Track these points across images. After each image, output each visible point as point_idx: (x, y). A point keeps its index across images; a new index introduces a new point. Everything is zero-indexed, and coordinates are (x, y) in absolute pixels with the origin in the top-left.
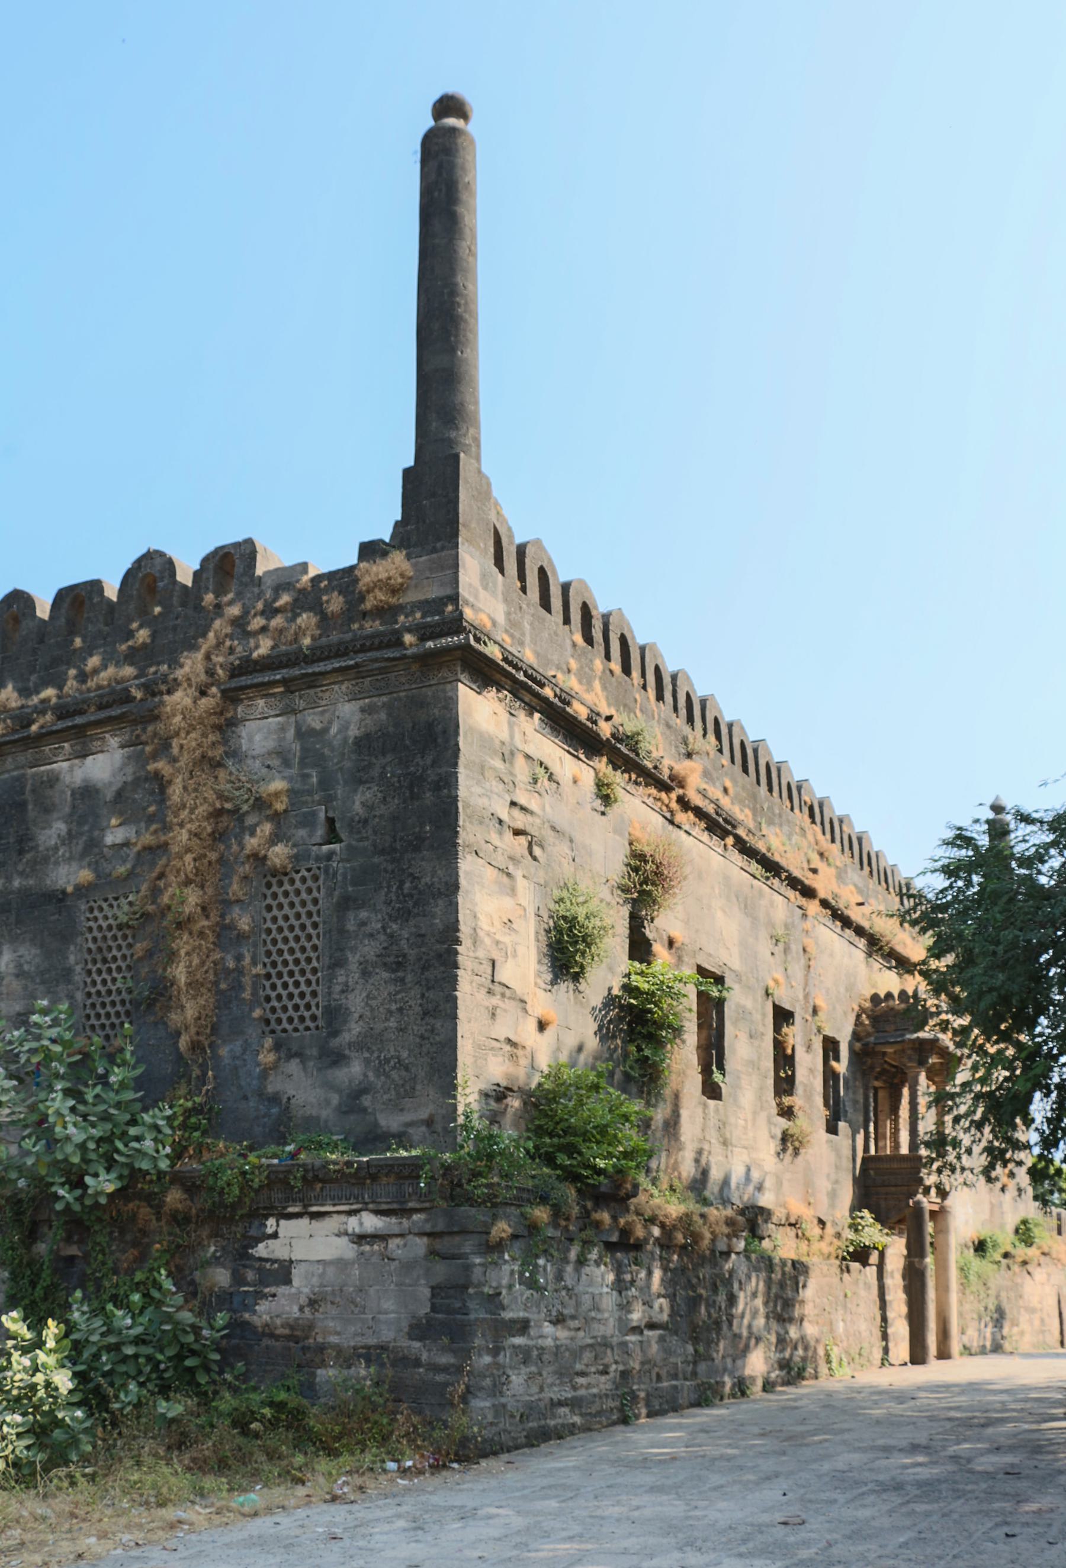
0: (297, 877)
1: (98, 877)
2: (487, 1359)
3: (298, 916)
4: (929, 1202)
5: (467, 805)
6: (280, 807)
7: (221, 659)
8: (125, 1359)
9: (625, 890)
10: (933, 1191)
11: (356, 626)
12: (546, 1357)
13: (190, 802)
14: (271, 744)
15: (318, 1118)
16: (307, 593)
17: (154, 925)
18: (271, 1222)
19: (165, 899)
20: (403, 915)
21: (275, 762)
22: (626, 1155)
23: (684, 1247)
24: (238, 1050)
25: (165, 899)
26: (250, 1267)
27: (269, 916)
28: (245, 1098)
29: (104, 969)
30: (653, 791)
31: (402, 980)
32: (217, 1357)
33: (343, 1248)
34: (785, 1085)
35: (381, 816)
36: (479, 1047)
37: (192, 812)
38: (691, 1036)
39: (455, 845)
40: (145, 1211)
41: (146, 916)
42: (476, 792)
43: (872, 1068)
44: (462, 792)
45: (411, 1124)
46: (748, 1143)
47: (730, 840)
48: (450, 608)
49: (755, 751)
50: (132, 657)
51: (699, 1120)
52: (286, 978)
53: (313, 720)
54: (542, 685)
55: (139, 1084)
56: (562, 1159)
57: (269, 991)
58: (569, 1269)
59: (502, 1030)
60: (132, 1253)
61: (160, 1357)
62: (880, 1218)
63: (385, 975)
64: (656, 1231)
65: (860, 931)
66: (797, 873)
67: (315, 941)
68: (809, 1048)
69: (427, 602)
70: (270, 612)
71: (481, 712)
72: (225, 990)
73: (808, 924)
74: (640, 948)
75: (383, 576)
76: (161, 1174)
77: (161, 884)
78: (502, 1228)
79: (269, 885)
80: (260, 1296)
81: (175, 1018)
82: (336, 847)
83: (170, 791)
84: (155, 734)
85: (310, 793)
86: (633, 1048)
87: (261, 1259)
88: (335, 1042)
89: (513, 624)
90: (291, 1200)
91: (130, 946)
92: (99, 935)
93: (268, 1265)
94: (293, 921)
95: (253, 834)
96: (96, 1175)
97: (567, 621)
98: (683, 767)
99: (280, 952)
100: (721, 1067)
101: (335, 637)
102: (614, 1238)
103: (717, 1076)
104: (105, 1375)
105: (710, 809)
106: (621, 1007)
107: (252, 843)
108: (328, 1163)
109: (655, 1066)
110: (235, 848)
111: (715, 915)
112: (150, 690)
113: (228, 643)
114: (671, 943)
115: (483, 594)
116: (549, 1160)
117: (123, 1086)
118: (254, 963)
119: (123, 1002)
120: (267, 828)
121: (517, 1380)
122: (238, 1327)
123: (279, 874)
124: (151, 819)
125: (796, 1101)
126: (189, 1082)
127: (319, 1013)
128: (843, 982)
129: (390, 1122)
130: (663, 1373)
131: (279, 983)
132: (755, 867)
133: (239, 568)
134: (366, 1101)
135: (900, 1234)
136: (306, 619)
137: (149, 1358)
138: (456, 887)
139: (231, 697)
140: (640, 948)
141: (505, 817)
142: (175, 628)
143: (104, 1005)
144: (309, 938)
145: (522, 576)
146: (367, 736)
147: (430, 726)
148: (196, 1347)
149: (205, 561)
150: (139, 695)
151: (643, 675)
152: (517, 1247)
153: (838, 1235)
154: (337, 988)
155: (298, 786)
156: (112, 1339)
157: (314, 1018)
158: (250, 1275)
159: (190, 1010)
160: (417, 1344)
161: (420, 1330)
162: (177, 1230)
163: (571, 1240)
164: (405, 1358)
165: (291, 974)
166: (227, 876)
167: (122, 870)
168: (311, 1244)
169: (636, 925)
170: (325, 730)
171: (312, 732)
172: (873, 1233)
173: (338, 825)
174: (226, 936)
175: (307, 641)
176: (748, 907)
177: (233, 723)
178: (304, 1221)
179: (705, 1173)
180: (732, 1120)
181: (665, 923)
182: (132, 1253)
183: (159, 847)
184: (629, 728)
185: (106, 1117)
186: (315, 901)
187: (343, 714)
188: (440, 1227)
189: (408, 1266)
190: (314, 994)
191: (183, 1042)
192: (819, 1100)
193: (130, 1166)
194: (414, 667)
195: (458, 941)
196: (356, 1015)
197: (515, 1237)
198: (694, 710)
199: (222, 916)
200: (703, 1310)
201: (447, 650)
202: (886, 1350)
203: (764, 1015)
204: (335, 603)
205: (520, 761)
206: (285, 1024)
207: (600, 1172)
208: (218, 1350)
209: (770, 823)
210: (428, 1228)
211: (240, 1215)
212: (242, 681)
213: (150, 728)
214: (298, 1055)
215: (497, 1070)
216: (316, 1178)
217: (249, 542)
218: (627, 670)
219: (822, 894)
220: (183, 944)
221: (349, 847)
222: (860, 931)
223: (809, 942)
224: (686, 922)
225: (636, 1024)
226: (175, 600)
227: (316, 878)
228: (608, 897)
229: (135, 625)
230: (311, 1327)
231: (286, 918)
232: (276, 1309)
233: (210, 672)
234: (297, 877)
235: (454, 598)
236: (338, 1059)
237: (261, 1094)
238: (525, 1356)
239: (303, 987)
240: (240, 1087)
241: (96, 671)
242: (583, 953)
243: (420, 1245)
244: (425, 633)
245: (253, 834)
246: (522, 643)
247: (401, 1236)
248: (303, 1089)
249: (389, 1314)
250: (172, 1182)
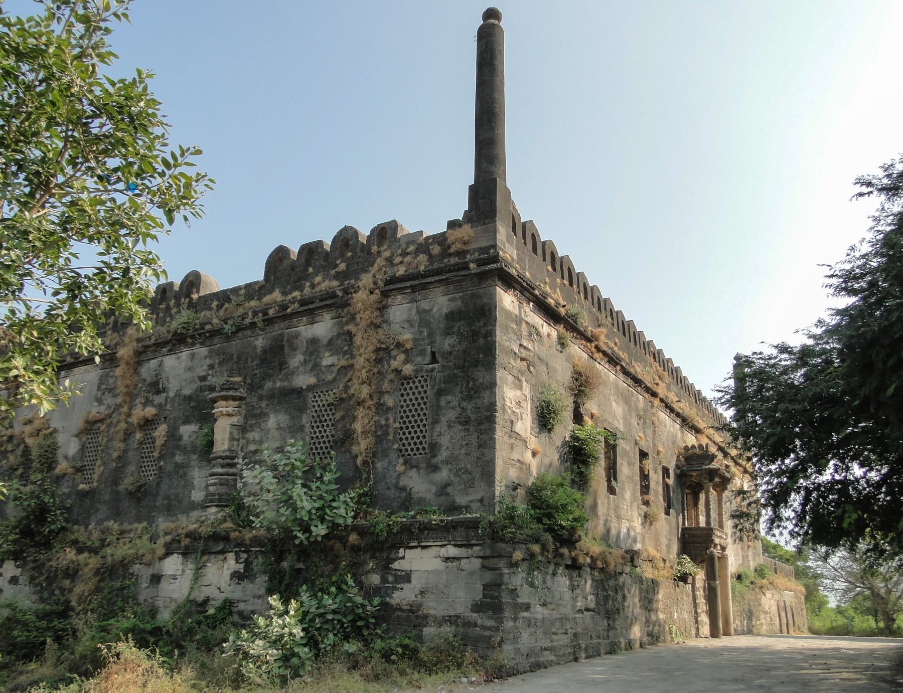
0: (416, 380)
1: (319, 381)
2: (511, 624)
3: (417, 399)
4: (716, 552)
5: (500, 345)
6: (408, 346)
7: (380, 277)
8: (327, 621)
9: (572, 389)
10: (719, 547)
11: (446, 260)
12: (538, 624)
13: (365, 346)
14: (404, 317)
15: (425, 499)
16: (422, 245)
17: (346, 404)
18: (401, 551)
19: (352, 391)
20: (469, 398)
21: (406, 325)
22: (575, 520)
23: (602, 569)
24: (386, 465)
25: (352, 391)
26: (390, 574)
27: (402, 399)
28: (389, 488)
29: (320, 425)
30: (584, 342)
31: (468, 429)
32: (373, 621)
33: (438, 564)
34: (645, 489)
35: (458, 351)
36: (505, 463)
37: (366, 349)
38: (602, 463)
39: (495, 364)
40: (338, 546)
41: (342, 400)
42: (504, 339)
43: (685, 483)
44: (498, 339)
45: (471, 502)
46: (629, 519)
47: (618, 368)
48: (492, 251)
49: (629, 326)
50: (337, 276)
51: (606, 505)
52: (410, 429)
53: (425, 305)
54: (534, 289)
55: (337, 481)
56: (545, 520)
57: (402, 436)
58: (549, 577)
59: (516, 456)
60: (331, 567)
61: (345, 620)
62: (694, 559)
63: (460, 427)
64: (588, 560)
65: (678, 415)
66: (649, 385)
67: (425, 411)
68: (656, 472)
69: (481, 248)
70: (405, 254)
71: (507, 300)
72: (380, 435)
73: (654, 411)
74: (578, 418)
75: (460, 236)
76: (346, 526)
77: (350, 384)
78: (518, 555)
79: (403, 384)
80: (395, 589)
81: (355, 449)
82: (436, 365)
83: (355, 339)
84: (348, 313)
85: (423, 340)
86: (576, 467)
87: (396, 570)
88: (434, 461)
89: (520, 260)
90: (411, 539)
91: (333, 414)
92: (318, 409)
93: (399, 573)
94: (414, 401)
95: (395, 359)
96: (316, 526)
97: (544, 260)
98: (596, 331)
99: (408, 417)
100: (615, 479)
101: (436, 266)
102: (569, 563)
103: (614, 483)
104: (317, 629)
105: (609, 352)
106: (570, 446)
107: (394, 364)
108: (431, 520)
109: (586, 476)
110: (386, 366)
112: (346, 292)
113: (384, 269)
114: (592, 416)
115: (507, 245)
116: (539, 521)
117: (330, 482)
118: (395, 422)
119: (329, 442)
120: (402, 357)
122: (384, 605)
123: (407, 378)
124: (345, 353)
125: (651, 498)
126: (361, 481)
127: (426, 446)
128: (671, 438)
129: (461, 500)
130: (593, 636)
131: (407, 432)
132: (629, 381)
133: (389, 234)
134: (449, 490)
135: (702, 568)
136: (422, 258)
137: (339, 621)
138: (495, 384)
139: (385, 294)
140: (578, 418)
141: (517, 351)
142: (358, 263)
143: (319, 443)
144: (422, 409)
145: (524, 238)
146: (452, 313)
147: (482, 307)
148: (363, 615)
149: (373, 231)
150: (340, 294)
151: (578, 287)
152: (525, 564)
153: (672, 567)
154: (436, 434)
155: (417, 337)
156: (321, 611)
157: (424, 449)
158: (391, 578)
159: (362, 446)
160: (476, 615)
161: (478, 608)
162: (354, 555)
163: (549, 563)
164: (469, 622)
165: (413, 427)
166: (382, 380)
167: (330, 377)
168: (422, 563)
170: (430, 310)
171: (425, 311)
172: (689, 566)
173: (437, 355)
174: (381, 408)
175: (422, 268)
176: (626, 400)
177: (385, 307)
178: (419, 549)
179: (608, 531)
180: (621, 505)
181: (591, 406)
182: (331, 567)
183: (349, 366)
184: (573, 311)
185: (321, 497)
186: (425, 392)
187: (440, 302)
188: (488, 553)
189: (471, 574)
190: (424, 437)
191: (359, 461)
192: (661, 498)
193: (333, 522)
194: (475, 279)
195: (496, 411)
196: (445, 448)
197: (524, 560)
198: (602, 305)
199: (379, 399)
200: (611, 602)
201: (492, 271)
202: (698, 629)
203: (635, 454)
204: (436, 250)
205: (524, 325)
206: (409, 452)
207: (563, 528)
208: (373, 617)
209: (636, 361)
210: (481, 554)
211: (384, 546)
212: (391, 287)
213: (346, 310)
214: (417, 467)
215: (513, 474)
216: (426, 528)
217: (395, 221)
218: (571, 284)
219: (661, 396)
220: (360, 413)
221: (443, 366)
222: (678, 415)
223: (654, 418)
224: (599, 406)
225: (577, 455)
226: (358, 249)
227: (426, 381)
228: (564, 392)
229: (338, 262)
230: (421, 605)
231: (411, 400)
232: (403, 596)
233: (375, 283)
234: (416, 380)
235: (494, 246)
236: (435, 468)
237: (396, 486)
238: (529, 623)
239: (419, 433)
240: (386, 483)
241: (319, 284)
242: (554, 419)
243: (477, 563)
244: (480, 263)
245: (395, 359)
246: (524, 269)
247: (468, 558)
248: (418, 484)
249: (461, 597)
250: (352, 530)
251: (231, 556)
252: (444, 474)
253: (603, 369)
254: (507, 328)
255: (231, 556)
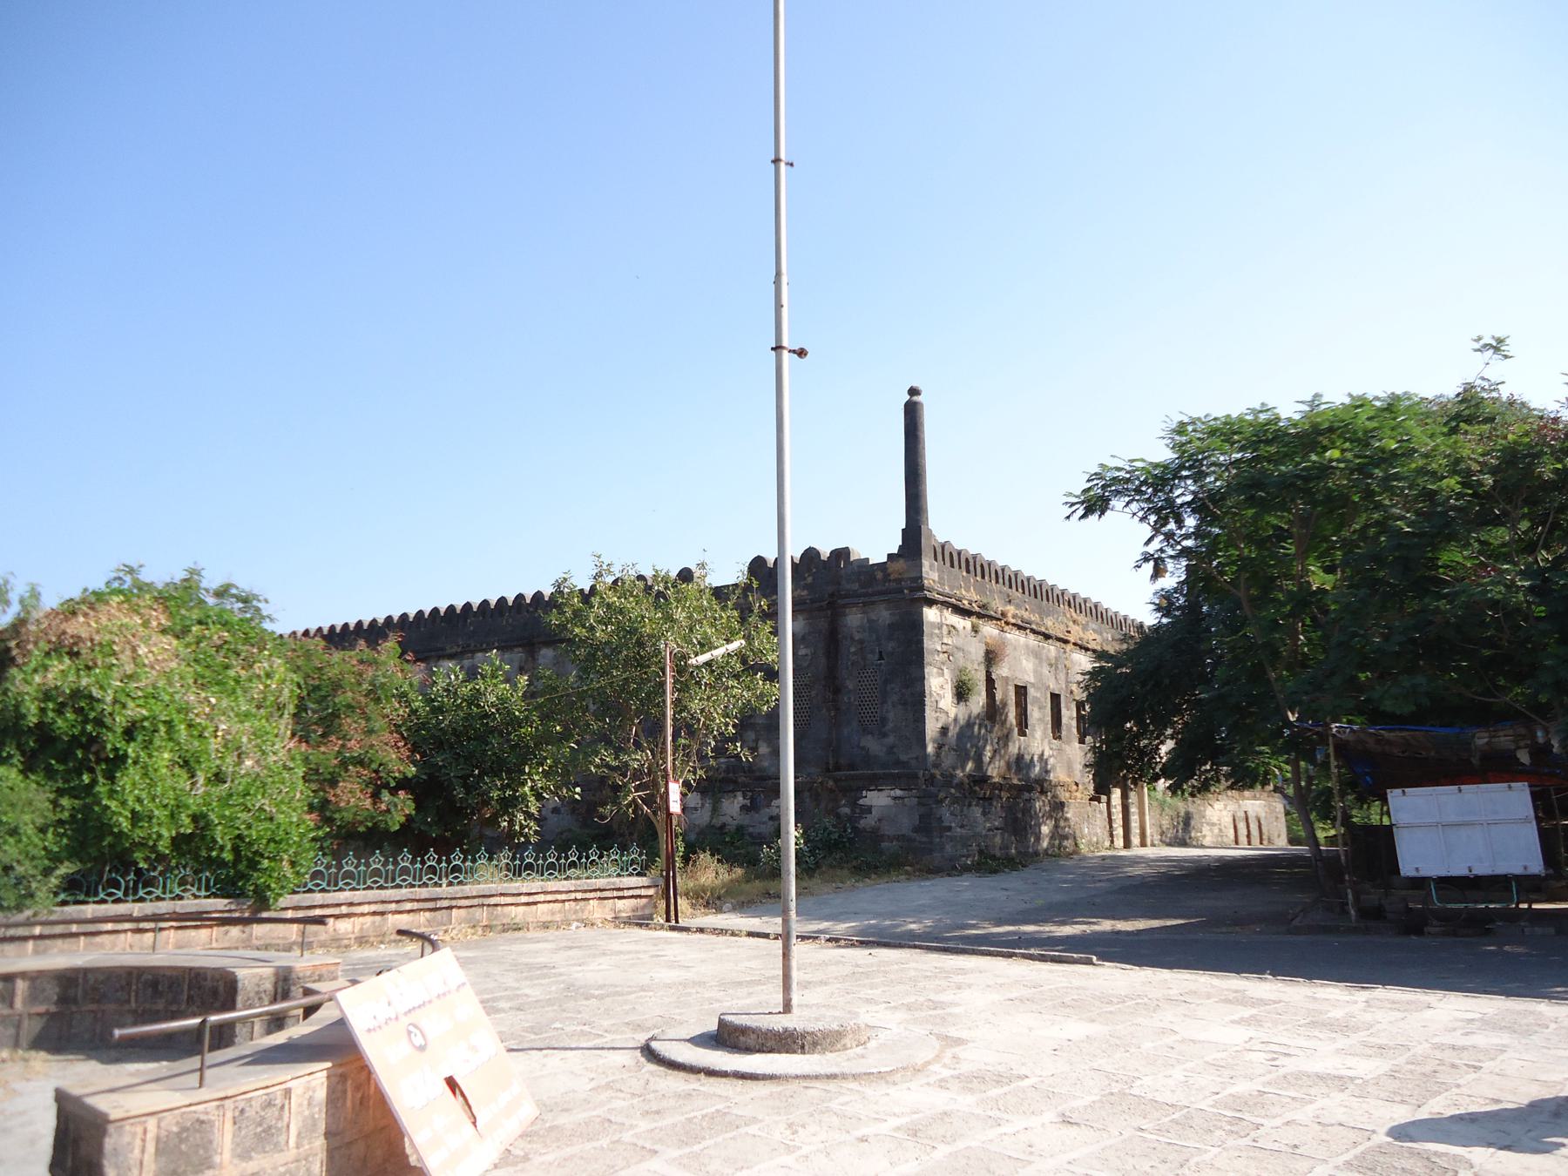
33: (889, 801)
42: (930, 644)
71: (931, 614)
111: (1024, 662)
121: (948, 848)
129: (904, 757)
161: (916, 830)
168: (878, 800)
169: (989, 675)
176: (1037, 654)
192: (1075, 731)
232: (868, 822)
236: (885, 735)
238: (952, 839)
248: (873, 745)
249: (906, 824)
251: (739, 794)
252: (891, 740)
253: (1014, 636)
254: (932, 634)
255: (739, 794)
